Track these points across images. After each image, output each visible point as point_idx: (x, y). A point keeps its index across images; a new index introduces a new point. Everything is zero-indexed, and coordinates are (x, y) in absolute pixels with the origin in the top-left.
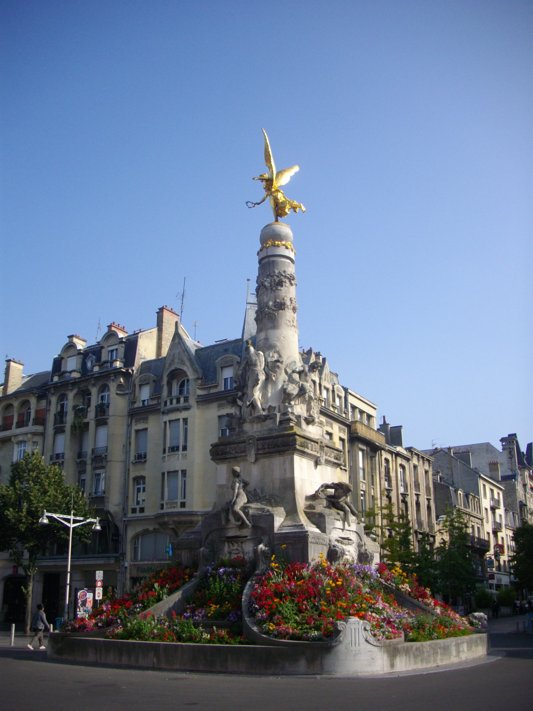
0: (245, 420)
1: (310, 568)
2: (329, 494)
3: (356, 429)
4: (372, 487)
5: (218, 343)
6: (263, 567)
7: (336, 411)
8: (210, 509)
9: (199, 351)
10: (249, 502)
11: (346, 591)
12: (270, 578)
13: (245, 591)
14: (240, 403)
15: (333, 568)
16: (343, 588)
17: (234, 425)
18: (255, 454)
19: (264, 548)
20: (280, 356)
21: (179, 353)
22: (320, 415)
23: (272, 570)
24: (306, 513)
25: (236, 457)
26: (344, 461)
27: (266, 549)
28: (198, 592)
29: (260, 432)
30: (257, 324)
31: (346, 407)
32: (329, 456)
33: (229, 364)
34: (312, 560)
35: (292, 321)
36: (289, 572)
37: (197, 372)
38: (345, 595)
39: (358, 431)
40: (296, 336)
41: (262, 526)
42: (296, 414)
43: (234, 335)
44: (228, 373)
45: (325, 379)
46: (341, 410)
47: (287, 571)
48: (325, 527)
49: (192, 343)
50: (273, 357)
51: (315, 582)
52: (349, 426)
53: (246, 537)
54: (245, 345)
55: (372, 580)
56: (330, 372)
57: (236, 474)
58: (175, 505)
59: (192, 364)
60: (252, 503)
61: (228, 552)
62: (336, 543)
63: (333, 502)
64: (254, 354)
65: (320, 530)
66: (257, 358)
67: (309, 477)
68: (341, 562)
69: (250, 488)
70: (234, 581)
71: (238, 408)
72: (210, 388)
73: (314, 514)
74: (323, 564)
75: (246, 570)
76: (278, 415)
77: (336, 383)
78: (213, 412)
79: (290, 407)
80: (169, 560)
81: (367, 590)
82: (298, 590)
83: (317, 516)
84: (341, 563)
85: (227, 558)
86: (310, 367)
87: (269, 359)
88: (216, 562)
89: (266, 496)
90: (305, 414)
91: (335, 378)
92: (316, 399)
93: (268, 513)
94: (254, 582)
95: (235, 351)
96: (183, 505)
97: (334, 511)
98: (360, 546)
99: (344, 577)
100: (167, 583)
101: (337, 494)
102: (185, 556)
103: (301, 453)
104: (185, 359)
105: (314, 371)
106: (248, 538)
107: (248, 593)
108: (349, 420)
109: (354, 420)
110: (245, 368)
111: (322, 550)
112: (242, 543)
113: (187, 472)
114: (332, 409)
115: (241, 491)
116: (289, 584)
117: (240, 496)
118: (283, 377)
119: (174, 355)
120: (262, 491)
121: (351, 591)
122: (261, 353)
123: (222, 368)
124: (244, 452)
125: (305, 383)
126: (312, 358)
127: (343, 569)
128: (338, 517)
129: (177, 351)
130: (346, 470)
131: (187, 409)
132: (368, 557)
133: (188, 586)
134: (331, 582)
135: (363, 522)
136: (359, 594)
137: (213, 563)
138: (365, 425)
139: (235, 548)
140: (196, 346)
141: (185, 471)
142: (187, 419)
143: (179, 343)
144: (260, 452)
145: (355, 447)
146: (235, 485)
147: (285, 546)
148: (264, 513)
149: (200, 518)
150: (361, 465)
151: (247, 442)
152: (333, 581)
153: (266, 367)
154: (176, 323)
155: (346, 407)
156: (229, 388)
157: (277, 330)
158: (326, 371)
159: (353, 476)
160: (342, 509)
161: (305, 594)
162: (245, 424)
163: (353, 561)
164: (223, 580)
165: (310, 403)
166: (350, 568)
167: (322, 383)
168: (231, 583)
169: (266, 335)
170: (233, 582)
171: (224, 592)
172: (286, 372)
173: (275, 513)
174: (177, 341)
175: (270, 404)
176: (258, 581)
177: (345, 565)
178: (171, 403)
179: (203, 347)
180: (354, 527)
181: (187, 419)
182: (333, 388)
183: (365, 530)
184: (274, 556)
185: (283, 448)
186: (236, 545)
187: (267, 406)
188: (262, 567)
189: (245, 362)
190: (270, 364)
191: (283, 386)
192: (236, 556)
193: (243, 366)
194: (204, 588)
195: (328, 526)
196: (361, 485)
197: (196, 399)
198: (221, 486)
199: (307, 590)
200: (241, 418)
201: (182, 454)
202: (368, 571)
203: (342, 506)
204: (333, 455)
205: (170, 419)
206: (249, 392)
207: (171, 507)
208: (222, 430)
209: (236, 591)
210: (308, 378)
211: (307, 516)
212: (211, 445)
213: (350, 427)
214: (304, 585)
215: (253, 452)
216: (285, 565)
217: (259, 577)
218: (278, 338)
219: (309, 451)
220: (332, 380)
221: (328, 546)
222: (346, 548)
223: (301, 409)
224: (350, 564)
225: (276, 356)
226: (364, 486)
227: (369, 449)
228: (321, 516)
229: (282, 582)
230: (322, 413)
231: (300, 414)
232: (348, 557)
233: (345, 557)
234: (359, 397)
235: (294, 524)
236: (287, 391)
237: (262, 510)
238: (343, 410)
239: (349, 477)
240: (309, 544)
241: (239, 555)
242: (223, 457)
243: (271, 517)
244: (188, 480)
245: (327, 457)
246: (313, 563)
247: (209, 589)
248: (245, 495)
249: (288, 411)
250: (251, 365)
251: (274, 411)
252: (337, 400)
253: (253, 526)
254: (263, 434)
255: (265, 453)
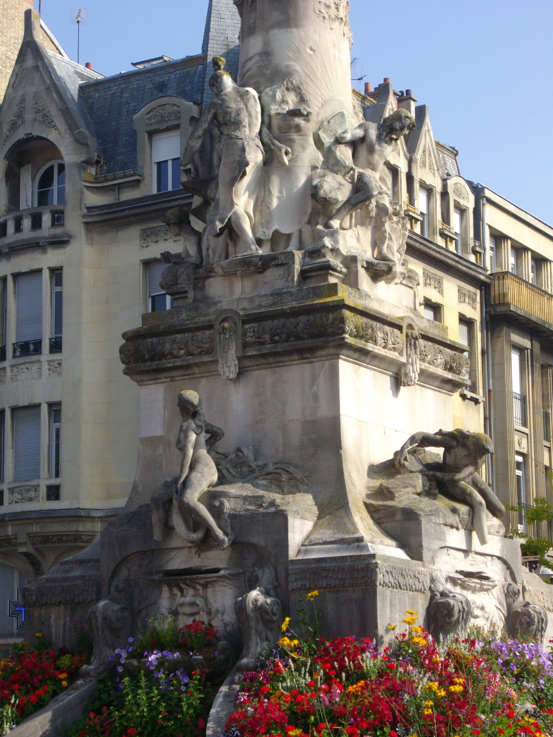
0: (212, 271)
1: (382, 650)
2: (430, 461)
3: (504, 295)
4: (547, 444)
5: (141, 67)
6: (259, 649)
7: (452, 248)
8: (120, 503)
9: (89, 88)
10: (222, 480)
11: (474, 708)
12: (277, 676)
13: (213, 711)
14: (197, 224)
15: (442, 650)
16: (466, 703)
17: (184, 283)
18: (239, 359)
19: (261, 599)
20: (302, 100)
21: (36, 95)
22: (409, 258)
23: (284, 655)
24: (371, 510)
25: (188, 367)
26: (472, 374)
27: (269, 601)
28: (92, 715)
29: (251, 300)
30: (241, 15)
31: (478, 235)
32: (431, 363)
33: (169, 124)
34: (387, 631)
35: (333, 6)
36: (327, 661)
37: (86, 145)
38: (472, 719)
39: (509, 299)
40: (345, 45)
41: (256, 543)
42: (344, 252)
43: (181, 45)
44: (167, 148)
45: (424, 164)
46: (465, 244)
47: (320, 658)
48: (420, 546)
49: (69, 68)
50: (284, 101)
51: (394, 686)
52: (484, 287)
53: (217, 570)
54: (210, 72)
55: (542, 681)
56: (438, 144)
57: (188, 410)
58: (32, 494)
59: (71, 126)
60: (230, 483)
61: (168, 611)
62: (449, 586)
63: (442, 482)
64: (233, 95)
65: (408, 553)
66: (242, 106)
67: (378, 416)
68: (463, 636)
69: (226, 444)
70: (186, 685)
71: (193, 239)
72: (120, 187)
73: (392, 512)
74: (416, 640)
75: (215, 656)
76: (298, 255)
77: (453, 172)
78: (130, 251)
79: (328, 235)
80: (19, 635)
81: (530, 706)
82: (350, 706)
83: (399, 516)
84: (462, 638)
85: (166, 626)
86: (380, 128)
87: (274, 109)
88: (140, 636)
89: (265, 465)
90: (366, 253)
91: (449, 161)
92: (396, 214)
93: (273, 509)
94: (237, 687)
95: (185, 89)
96: (54, 492)
97: (442, 503)
98: (510, 594)
99: (469, 673)
100: (13, 692)
101: (449, 460)
102: (58, 623)
103: (356, 355)
104: (53, 111)
105: (392, 139)
106: (222, 572)
107: (222, 714)
108: (485, 269)
109: (499, 270)
110: (209, 132)
111: (413, 603)
112: (205, 586)
113: (64, 408)
114: (440, 241)
115: (203, 452)
116: (328, 691)
117: (199, 467)
118: (310, 155)
119: (23, 101)
120: (257, 453)
121: (487, 709)
122: (252, 91)
123: (151, 134)
124: (210, 351)
125: (368, 172)
126: (389, 107)
127: (466, 653)
128: (453, 519)
129: (30, 90)
130: (476, 401)
131: (60, 242)
132: (530, 623)
133: (66, 699)
134: (435, 685)
135: (522, 536)
136: (509, 716)
137: (131, 640)
138: (527, 283)
139: (188, 599)
140: (81, 75)
141: (59, 404)
142: (61, 269)
143: (37, 68)
144: (252, 352)
145: (502, 343)
146: (186, 437)
147: (316, 593)
148: (261, 510)
149: (98, 527)
150: (516, 388)
151: (217, 327)
152: (441, 684)
153: (265, 130)
154: (28, 13)
155: (478, 235)
156: (170, 189)
157: (294, 30)
158: (427, 140)
159: (495, 416)
160: (463, 498)
161: (367, 717)
162: (212, 280)
163: (493, 633)
164: (157, 682)
165: (383, 224)
166: (484, 651)
167: (414, 173)
168: (178, 689)
169: (266, 43)
170: (183, 688)
171: (160, 713)
172: (318, 143)
173: (290, 510)
174: (30, 62)
175: (275, 227)
176: (246, 684)
177: (473, 643)
178: (18, 228)
179: (100, 77)
180: (495, 544)
181: (61, 269)
182: (445, 186)
183: (524, 554)
184: (287, 619)
185: (309, 342)
186: (191, 592)
187: (269, 234)
188: (257, 647)
189: (210, 117)
190: (275, 122)
191: (310, 180)
192: (189, 621)
193: (205, 126)
194: (109, 704)
195: (428, 543)
196: (516, 438)
197: (84, 216)
198: (150, 442)
199: (373, 705)
200: (198, 266)
201: (49, 361)
202: (532, 659)
203: (464, 491)
204: (440, 360)
205: (17, 270)
206: (221, 195)
207: (23, 500)
208: (153, 298)
209: (191, 711)
210: (376, 157)
211: (373, 518)
212: (124, 335)
213: (486, 287)
214: (367, 694)
215: (232, 353)
216: (316, 643)
217: (250, 674)
218: (298, 51)
219: (378, 350)
220: (441, 166)
221: (429, 594)
222: (476, 599)
223: (358, 240)
224: (484, 640)
225: (292, 101)
226: (524, 442)
227: (537, 346)
228: (410, 515)
229: (309, 685)
230: (412, 250)
231: (354, 252)
232: (479, 622)
233: (472, 622)
234: (512, 209)
235: (339, 536)
236: (321, 193)
237: (257, 500)
238: (471, 243)
239: (485, 419)
240: (379, 589)
241: (198, 618)
242: (154, 365)
243: (280, 520)
244: (66, 428)
245: (425, 365)
246: (388, 639)
247: (121, 706)
248: (213, 464)
249: (324, 246)
250: (226, 124)
251: (288, 246)
252: (455, 217)
253: (234, 544)
254: (260, 306)
255: (263, 356)
